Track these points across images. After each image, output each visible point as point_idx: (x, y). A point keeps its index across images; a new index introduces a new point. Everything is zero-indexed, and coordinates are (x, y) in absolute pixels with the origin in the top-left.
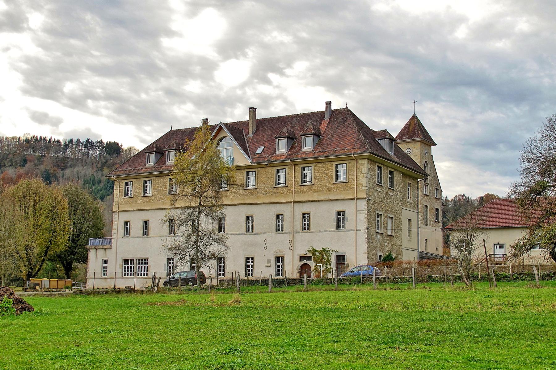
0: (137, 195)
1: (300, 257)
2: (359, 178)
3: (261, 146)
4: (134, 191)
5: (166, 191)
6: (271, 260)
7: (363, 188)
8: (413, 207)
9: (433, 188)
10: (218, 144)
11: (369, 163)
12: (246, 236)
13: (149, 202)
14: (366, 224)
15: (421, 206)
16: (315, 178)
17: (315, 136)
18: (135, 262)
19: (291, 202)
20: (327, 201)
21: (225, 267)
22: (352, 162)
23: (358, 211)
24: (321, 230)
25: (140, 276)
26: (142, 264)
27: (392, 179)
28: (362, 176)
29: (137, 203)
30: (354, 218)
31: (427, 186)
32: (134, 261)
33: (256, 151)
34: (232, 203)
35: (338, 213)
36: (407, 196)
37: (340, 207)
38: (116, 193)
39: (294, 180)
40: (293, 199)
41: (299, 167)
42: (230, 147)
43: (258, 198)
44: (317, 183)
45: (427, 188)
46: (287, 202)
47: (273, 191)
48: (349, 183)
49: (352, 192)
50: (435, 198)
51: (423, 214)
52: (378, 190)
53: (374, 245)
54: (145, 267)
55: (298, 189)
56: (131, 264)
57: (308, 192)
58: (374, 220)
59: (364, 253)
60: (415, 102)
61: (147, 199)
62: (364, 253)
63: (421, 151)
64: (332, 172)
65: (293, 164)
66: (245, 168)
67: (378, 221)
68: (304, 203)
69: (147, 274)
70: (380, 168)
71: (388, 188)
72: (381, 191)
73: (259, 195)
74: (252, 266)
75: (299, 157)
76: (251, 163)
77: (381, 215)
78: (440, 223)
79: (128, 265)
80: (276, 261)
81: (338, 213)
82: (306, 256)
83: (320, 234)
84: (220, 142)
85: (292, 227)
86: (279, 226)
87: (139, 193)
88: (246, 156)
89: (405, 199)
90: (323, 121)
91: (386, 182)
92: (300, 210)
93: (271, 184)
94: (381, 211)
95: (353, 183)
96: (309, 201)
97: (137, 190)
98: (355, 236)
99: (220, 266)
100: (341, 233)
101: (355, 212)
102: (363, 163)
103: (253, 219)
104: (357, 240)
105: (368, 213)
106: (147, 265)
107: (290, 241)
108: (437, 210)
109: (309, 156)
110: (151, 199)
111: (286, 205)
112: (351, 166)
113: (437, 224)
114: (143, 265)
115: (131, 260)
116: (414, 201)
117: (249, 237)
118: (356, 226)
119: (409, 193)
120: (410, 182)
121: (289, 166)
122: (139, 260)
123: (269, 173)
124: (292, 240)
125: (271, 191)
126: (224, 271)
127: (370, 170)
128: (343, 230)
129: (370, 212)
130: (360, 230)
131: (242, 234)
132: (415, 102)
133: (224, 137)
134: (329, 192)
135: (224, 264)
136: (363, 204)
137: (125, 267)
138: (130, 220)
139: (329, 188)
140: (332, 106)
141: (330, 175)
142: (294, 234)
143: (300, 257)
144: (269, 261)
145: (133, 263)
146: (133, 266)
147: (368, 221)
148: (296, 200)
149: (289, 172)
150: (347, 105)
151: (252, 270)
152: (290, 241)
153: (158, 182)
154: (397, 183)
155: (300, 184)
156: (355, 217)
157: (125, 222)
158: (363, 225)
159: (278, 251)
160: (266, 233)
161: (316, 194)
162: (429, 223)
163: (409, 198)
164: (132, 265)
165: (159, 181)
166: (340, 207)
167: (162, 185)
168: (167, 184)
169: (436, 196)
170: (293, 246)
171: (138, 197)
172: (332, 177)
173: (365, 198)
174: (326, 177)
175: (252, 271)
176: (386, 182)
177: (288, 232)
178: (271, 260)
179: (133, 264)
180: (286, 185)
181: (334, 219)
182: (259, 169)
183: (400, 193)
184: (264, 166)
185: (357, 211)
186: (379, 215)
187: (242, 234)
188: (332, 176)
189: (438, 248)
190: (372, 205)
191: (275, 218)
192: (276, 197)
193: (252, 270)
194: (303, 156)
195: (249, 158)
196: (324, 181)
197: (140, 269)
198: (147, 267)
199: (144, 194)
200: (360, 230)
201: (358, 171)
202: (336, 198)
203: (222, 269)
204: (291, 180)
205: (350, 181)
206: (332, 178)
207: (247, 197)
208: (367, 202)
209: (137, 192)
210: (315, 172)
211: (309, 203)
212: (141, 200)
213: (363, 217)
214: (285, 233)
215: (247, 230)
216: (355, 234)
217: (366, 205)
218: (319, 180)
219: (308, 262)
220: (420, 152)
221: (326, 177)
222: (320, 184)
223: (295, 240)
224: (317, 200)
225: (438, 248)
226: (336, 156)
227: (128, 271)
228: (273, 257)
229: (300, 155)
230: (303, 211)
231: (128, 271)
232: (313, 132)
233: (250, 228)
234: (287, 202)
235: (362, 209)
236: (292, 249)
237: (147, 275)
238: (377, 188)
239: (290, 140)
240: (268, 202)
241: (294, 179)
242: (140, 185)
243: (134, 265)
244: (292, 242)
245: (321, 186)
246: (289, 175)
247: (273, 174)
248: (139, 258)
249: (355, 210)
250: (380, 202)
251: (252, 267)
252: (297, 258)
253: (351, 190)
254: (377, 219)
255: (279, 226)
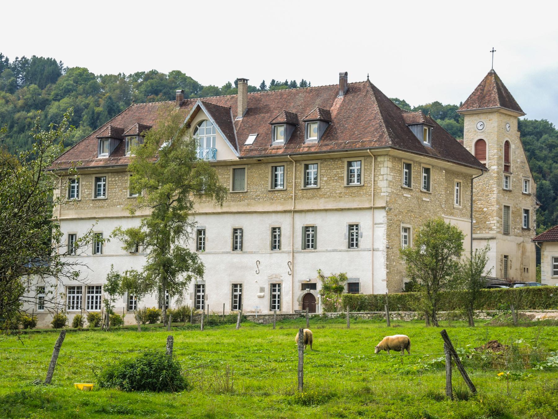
0: (85, 198)
1: (303, 285)
2: (377, 181)
3: (252, 132)
4: (82, 192)
5: (126, 193)
6: (264, 288)
7: (382, 194)
8: (463, 215)
9: (519, 180)
10: (196, 130)
11: (391, 160)
12: (233, 255)
13: (102, 207)
14: (385, 242)
15: (498, 206)
16: (322, 179)
17: (321, 122)
18: (83, 290)
19: (290, 212)
20: (337, 210)
21: (205, 297)
22: (368, 159)
23: (376, 224)
24: (329, 249)
25: (75, 310)
26: (93, 293)
27: (427, 179)
28: (381, 177)
29: (86, 208)
30: (371, 233)
31: (510, 176)
32: (81, 289)
33: (245, 141)
34: (215, 211)
35: (351, 227)
36: (453, 200)
37: (353, 218)
38: (57, 194)
39: (295, 182)
40: (293, 207)
41: (301, 164)
42: (212, 135)
43: (248, 205)
44: (324, 186)
45: (508, 180)
46: (285, 212)
47: (267, 195)
48: (364, 188)
49: (368, 200)
50: (523, 194)
51: (502, 219)
52: (405, 195)
53: (397, 269)
54: (97, 297)
55: (300, 193)
56: (78, 293)
57: (312, 198)
58: (398, 236)
59: (383, 280)
60: (493, 51)
61: (100, 204)
62: (383, 280)
63: (498, 126)
64: (343, 172)
65: (292, 160)
66: (231, 164)
67: (405, 237)
68: (307, 213)
69: (100, 306)
70: (408, 166)
71: (421, 192)
72: (409, 196)
73: (249, 200)
74: (279, 295)
75: (301, 150)
76: (240, 158)
77: (409, 228)
78: (531, 231)
79: (92, 295)
80: (232, 289)
81: (351, 227)
82: (309, 283)
83: (328, 254)
84: (198, 127)
85: (292, 244)
86: (275, 244)
87: (89, 194)
88: (232, 148)
89: (449, 204)
90: (336, 100)
91: (418, 182)
92: (302, 221)
93: (265, 186)
94: (409, 223)
95: (370, 187)
96: (313, 211)
97: (86, 190)
98: (371, 258)
99: (198, 296)
100: (353, 253)
101: (372, 226)
102: (383, 160)
103: (242, 233)
104: (374, 263)
105: (389, 226)
106: (100, 295)
107: (289, 263)
108: (527, 211)
109: (313, 150)
110: (105, 204)
111: (284, 215)
112: (367, 164)
113: (526, 233)
114: (95, 295)
115: (97, 287)
116: (465, 206)
117: (237, 258)
118: (373, 245)
119: (457, 195)
120: (459, 181)
121: (288, 163)
122: (89, 287)
123: (263, 171)
124: (291, 261)
125: (265, 195)
126: (203, 302)
127: (392, 169)
128: (357, 249)
129: (390, 225)
130: (377, 250)
131: (227, 253)
132: (493, 51)
133: (204, 121)
134: (340, 199)
135: (203, 294)
136: (381, 216)
137: (70, 297)
138: (77, 232)
139: (339, 193)
140: (348, 78)
141: (340, 175)
142: (295, 254)
143: (303, 285)
144: (262, 290)
145: (81, 291)
146: (81, 297)
147: (388, 236)
148: (299, 208)
149: (288, 170)
150: (368, 77)
151: (279, 301)
152: (289, 263)
153: (115, 181)
154: (436, 184)
155: (303, 188)
156: (372, 232)
157: (69, 235)
158: (381, 243)
159: (274, 276)
160: (259, 252)
161: (323, 200)
162: (511, 231)
163: (457, 203)
164: (80, 295)
165: (117, 179)
166: (353, 218)
167: (120, 184)
168: (127, 182)
169: (526, 191)
170: (293, 269)
171: (88, 200)
172: (342, 178)
173: (384, 208)
174: (336, 178)
175: (278, 303)
176: (418, 182)
177: (286, 251)
178: (264, 288)
179: (81, 293)
180: (285, 189)
181: (345, 235)
182: (249, 166)
183: (441, 198)
184: (255, 162)
185: (375, 224)
186: (406, 230)
187: (227, 253)
188: (342, 177)
189: (527, 269)
190: (396, 215)
191: (269, 232)
192: (272, 204)
193: (279, 302)
194: (306, 149)
195: (236, 149)
196: (333, 184)
197: (90, 300)
198: (100, 297)
199: (96, 197)
200: (377, 250)
201: (376, 171)
202: (347, 207)
203: (201, 300)
204: (291, 181)
205: (366, 185)
206: (343, 180)
207: (234, 203)
208: (387, 212)
209: (86, 193)
210: (322, 171)
211: (314, 213)
212: (91, 205)
213: (381, 232)
214: (283, 252)
215: (235, 248)
216: (371, 256)
217: (385, 216)
218: (326, 181)
219: (312, 291)
220: (498, 127)
221: (336, 178)
222: (328, 187)
223: (295, 262)
224: (323, 208)
225: (527, 269)
226: (347, 151)
227: (78, 303)
228: (267, 284)
229: (302, 149)
230: (306, 223)
231: (78, 303)
232: (319, 117)
233: (239, 245)
234: (285, 212)
235: (381, 222)
236: (292, 274)
237: (100, 308)
238: (404, 192)
239: (291, 127)
240: (260, 209)
241: (295, 179)
242: (90, 183)
243: (81, 295)
244: (291, 264)
245: (328, 190)
246: (288, 175)
247: (268, 173)
248: (98, 285)
249: (371, 223)
250: (409, 211)
251: (279, 298)
252: (298, 286)
253: (366, 197)
254: (403, 234)
255: (275, 244)
